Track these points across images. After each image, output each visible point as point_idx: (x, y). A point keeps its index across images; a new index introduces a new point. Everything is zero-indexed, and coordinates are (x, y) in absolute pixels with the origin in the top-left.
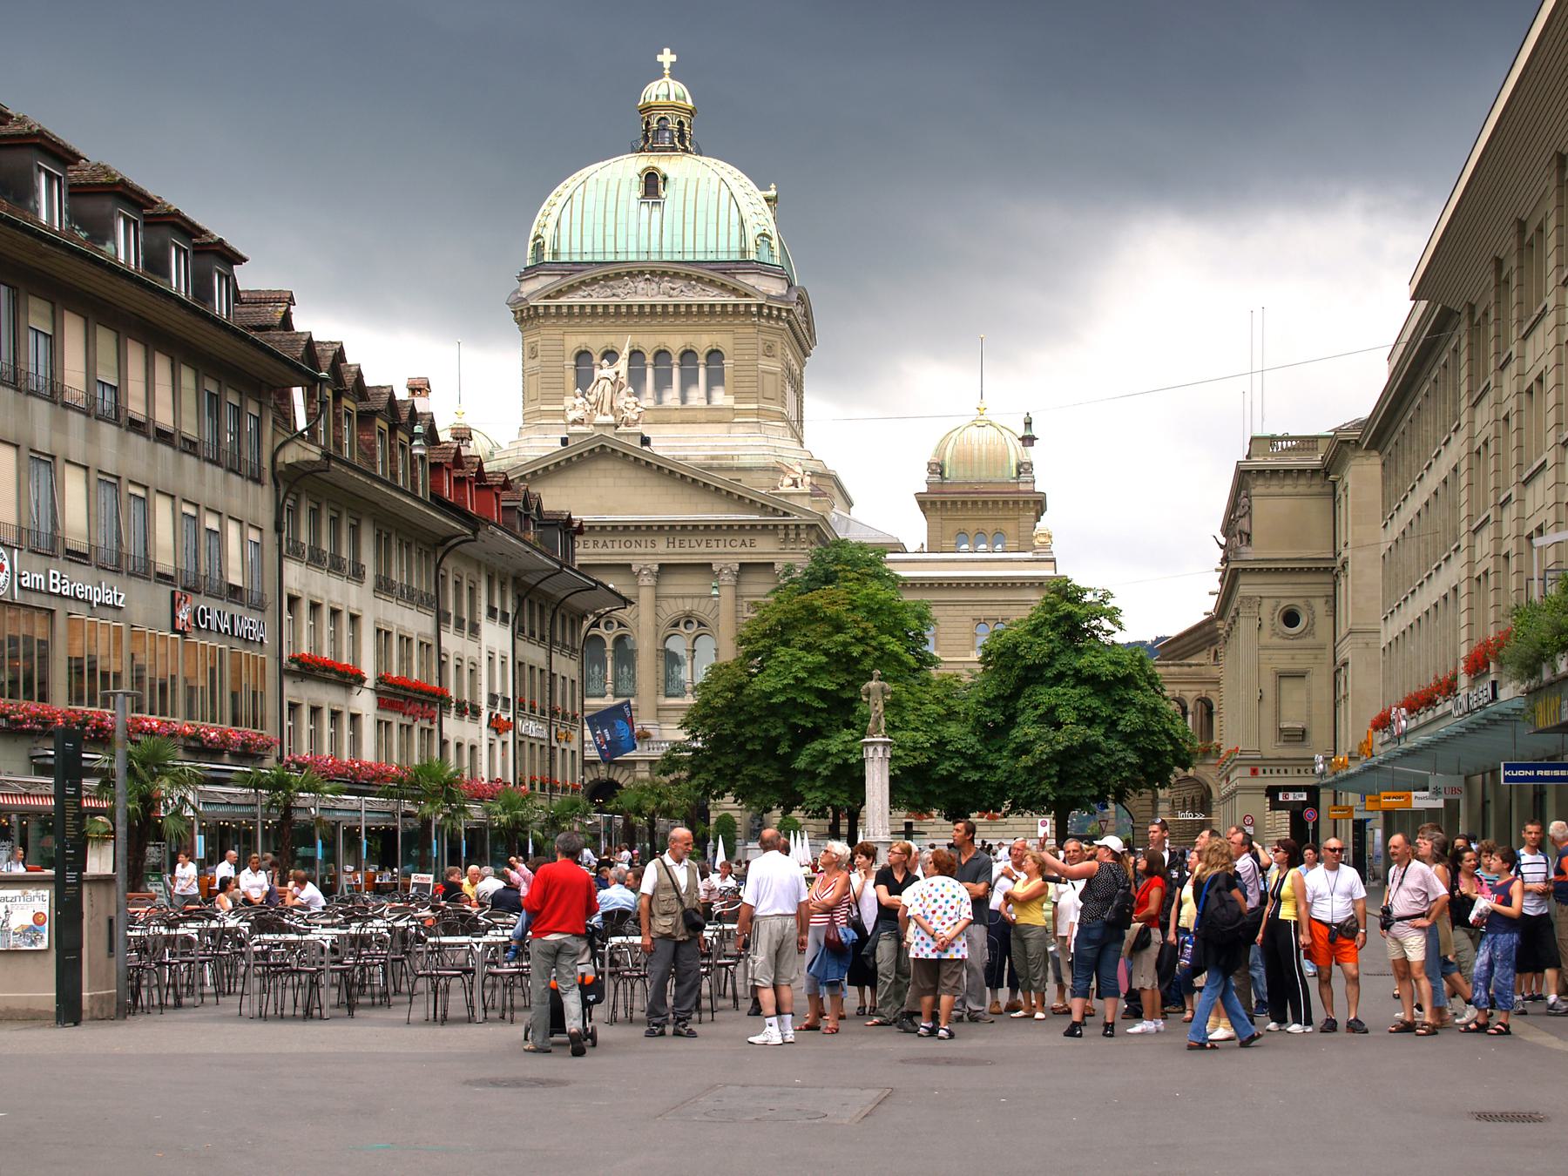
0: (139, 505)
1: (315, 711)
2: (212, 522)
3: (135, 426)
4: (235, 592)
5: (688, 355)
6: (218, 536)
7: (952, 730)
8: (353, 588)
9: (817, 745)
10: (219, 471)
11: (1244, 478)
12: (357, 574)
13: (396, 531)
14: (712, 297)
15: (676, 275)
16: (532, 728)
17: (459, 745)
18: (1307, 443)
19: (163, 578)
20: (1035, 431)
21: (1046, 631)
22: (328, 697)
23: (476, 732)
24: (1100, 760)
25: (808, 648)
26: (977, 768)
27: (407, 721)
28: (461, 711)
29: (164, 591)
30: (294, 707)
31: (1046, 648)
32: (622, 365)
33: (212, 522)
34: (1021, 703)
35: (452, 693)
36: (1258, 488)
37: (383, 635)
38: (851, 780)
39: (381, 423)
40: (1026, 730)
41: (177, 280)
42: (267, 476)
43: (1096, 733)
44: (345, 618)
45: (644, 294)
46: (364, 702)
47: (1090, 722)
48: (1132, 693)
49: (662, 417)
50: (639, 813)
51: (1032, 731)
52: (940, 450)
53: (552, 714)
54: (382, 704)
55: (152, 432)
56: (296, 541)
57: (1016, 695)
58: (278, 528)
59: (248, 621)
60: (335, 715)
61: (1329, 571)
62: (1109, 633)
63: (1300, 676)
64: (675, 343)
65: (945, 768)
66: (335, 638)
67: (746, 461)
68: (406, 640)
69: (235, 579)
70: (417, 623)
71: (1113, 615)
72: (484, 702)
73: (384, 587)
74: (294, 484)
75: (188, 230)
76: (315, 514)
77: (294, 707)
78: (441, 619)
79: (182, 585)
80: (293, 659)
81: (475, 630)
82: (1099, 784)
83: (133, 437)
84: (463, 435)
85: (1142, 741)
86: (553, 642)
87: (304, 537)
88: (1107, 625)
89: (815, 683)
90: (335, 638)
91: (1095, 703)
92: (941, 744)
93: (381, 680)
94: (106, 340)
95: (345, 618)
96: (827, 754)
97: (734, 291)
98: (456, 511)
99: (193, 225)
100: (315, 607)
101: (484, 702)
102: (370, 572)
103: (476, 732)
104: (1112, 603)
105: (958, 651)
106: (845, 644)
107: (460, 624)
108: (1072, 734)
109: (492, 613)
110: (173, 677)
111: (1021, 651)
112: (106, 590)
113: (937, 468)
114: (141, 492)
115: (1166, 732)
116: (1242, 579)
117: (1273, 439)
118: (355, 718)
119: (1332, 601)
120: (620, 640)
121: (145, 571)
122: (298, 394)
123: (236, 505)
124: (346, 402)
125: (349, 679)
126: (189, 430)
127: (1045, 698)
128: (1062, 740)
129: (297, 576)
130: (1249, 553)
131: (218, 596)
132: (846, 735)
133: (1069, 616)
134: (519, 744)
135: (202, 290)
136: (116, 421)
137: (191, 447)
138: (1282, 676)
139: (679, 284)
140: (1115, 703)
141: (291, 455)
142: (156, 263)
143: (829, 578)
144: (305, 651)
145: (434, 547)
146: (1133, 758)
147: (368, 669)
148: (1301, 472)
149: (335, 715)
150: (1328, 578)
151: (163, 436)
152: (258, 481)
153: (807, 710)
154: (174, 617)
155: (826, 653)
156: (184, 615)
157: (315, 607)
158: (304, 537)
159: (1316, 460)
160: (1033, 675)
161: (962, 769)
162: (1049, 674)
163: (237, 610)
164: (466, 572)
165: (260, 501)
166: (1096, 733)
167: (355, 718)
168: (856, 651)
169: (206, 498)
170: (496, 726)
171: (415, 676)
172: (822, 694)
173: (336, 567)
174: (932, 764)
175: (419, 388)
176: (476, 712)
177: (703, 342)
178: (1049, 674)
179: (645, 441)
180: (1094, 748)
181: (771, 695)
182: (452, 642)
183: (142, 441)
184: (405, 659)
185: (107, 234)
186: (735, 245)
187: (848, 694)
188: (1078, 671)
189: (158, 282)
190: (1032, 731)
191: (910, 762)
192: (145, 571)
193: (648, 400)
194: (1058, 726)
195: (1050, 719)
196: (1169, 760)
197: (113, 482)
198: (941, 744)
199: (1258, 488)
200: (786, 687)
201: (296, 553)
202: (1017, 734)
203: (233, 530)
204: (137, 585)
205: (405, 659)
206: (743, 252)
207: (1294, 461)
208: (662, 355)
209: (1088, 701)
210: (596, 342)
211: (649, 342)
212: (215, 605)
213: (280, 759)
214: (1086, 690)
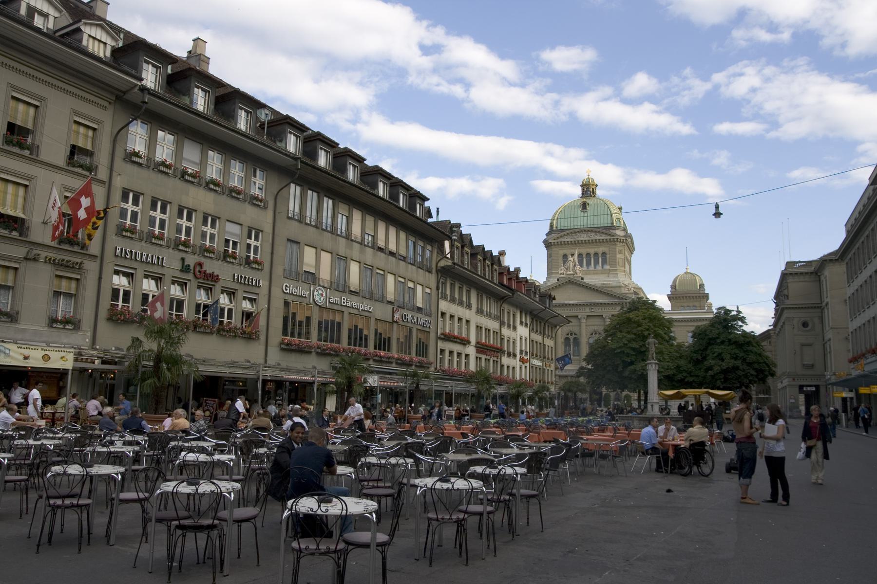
0: (381, 277)
1: (451, 353)
2: (411, 285)
3: (380, 249)
4: (419, 309)
5: (596, 254)
6: (414, 290)
7: (682, 362)
8: (467, 311)
9: (632, 367)
10: (414, 267)
11: (784, 276)
12: (469, 306)
13: (484, 291)
14: (604, 237)
15: (592, 231)
16: (537, 363)
17: (508, 367)
18: (809, 263)
19: (390, 302)
20: (721, 211)
21: (717, 326)
22: (456, 348)
23: (516, 363)
24: (741, 373)
25: (628, 332)
26: (691, 376)
27: (488, 357)
28: (509, 355)
29: (390, 307)
30: (442, 351)
31: (717, 331)
32: (576, 257)
33: (411, 285)
34: (708, 352)
35: (506, 349)
36: (790, 279)
37: (479, 328)
38: (643, 379)
39: (480, 257)
40: (711, 362)
41: (402, 202)
42: (434, 271)
43: (738, 363)
44: (464, 321)
45: (584, 237)
46: (471, 350)
47: (736, 358)
48: (751, 348)
49: (587, 273)
50: (570, 391)
51: (713, 362)
52: (675, 281)
53: (543, 358)
54: (477, 352)
55: (387, 252)
56: (445, 294)
57: (706, 349)
58: (438, 289)
59: (423, 319)
60: (459, 354)
61: (819, 308)
62: (741, 326)
63: (810, 345)
64: (592, 251)
65: (680, 377)
66: (460, 328)
67: (614, 285)
68: (488, 330)
69: (419, 304)
70: (493, 325)
71: (743, 319)
72: (518, 352)
73: (480, 311)
74: (445, 273)
75: (407, 188)
76: (453, 285)
77: (442, 351)
78: (502, 324)
79: (396, 305)
80: (442, 334)
81: (515, 328)
82: (740, 382)
83: (379, 253)
84: (518, 270)
85: (756, 366)
86: (544, 334)
87: (448, 292)
88: (740, 323)
89: (630, 345)
90: (460, 328)
91: (737, 351)
92: (678, 367)
93: (477, 343)
94: (370, 220)
95: (464, 321)
96: (635, 371)
97: (610, 235)
98: (508, 288)
99: (409, 186)
100: (452, 317)
101: (518, 352)
102: (474, 306)
103: (516, 363)
104: (742, 315)
105: (684, 337)
106: (642, 331)
107: (509, 326)
108: (729, 363)
109: (521, 323)
110: (389, 338)
111: (708, 333)
112: (365, 306)
113: (673, 287)
114: (403, 280)
115: (765, 362)
116: (785, 311)
117: (795, 263)
118: (467, 356)
119: (822, 319)
120: (575, 339)
121: (382, 299)
122: (447, 244)
123: (421, 279)
124: (466, 249)
125: (465, 342)
126: (403, 252)
127: (716, 350)
128: (725, 365)
129: (444, 305)
130: (788, 302)
131: (413, 310)
132: (642, 364)
133: (727, 320)
134: (532, 367)
135: (412, 207)
136: (372, 247)
137: (404, 259)
138: (803, 345)
139: (593, 234)
140: (745, 352)
141: (443, 263)
142: (394, 197)
143: (637, 309)
144: (447, 331)
145: (501, 299)
146: (753, 372)
147: (473, 339)
148: (807, 273)
149: (459, 354)
150: (819, 310)
151: (391, 254)
152: (430, 272)
153: (628, 355)
154: (393, 316)
155: (635, 334)
156: (397, 316)
157: (452, 317)
158: (448, 292)
159: (812, 269)
160: (711, 342)
161: (686, 377)
162: (718, 341)
163: (420, 315)
164: (512, 310)
165: (432, 279)
166: (738, 363)
167: (467, 356)
168: (646, 333)
169: (409, 275)
170: (522, 360)
171: (483, 341)
172: (634, 349)
173: (461, 303)
174: (674, 375)
175: (502, 253)
176: (515, 356)
177: (600, 250)
178: (718, 341)
179: (582, 279)
180: (737, 368)
181: (615, 350)
182: (506, 332)
183: (383, 255)
184: (488, 336)
185: (376, 187)
186: (609, 222)
187: (643, 349)
188: (730, 340)
189: (375, 192)
190: (713, 362)
191: (667, 374)
192: (382, 299)
193: (585, 268)
194: (723, 360)
195: (720, 357)
196: (767, 373)
197: (371, 268)
198: (678, 367)
199: (790, 279)
200: (620, 347)
201: (444, 297)
202: (707, 363)
203: (419, 289)
204: (378, 304)
205: (488, 336)
206: (612, 223)
207: (803, 270)
208: (588, 255)
209: (734, 351)
210: (567, 251)
211: (584, 251)
212: (410, 314)
213: (436, 369)
214: (734, 347)
